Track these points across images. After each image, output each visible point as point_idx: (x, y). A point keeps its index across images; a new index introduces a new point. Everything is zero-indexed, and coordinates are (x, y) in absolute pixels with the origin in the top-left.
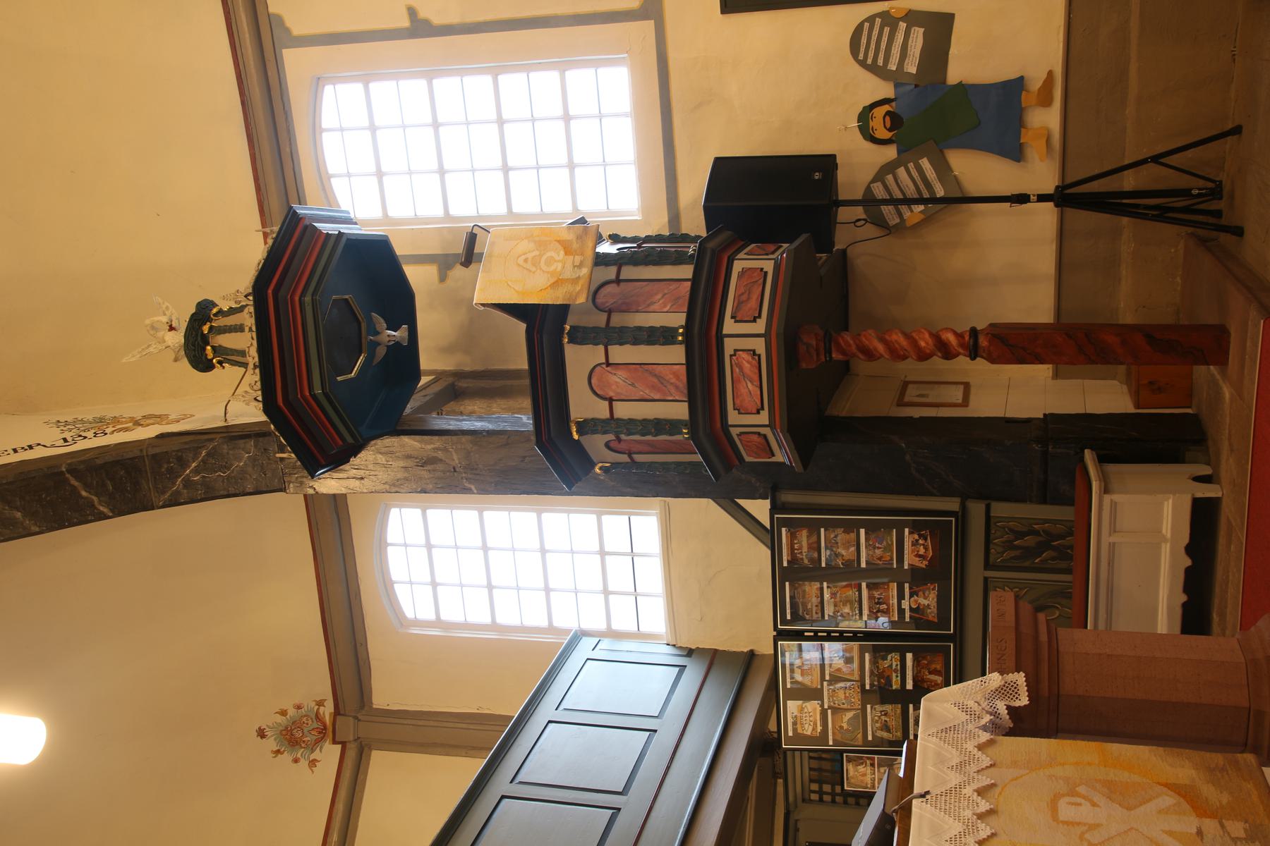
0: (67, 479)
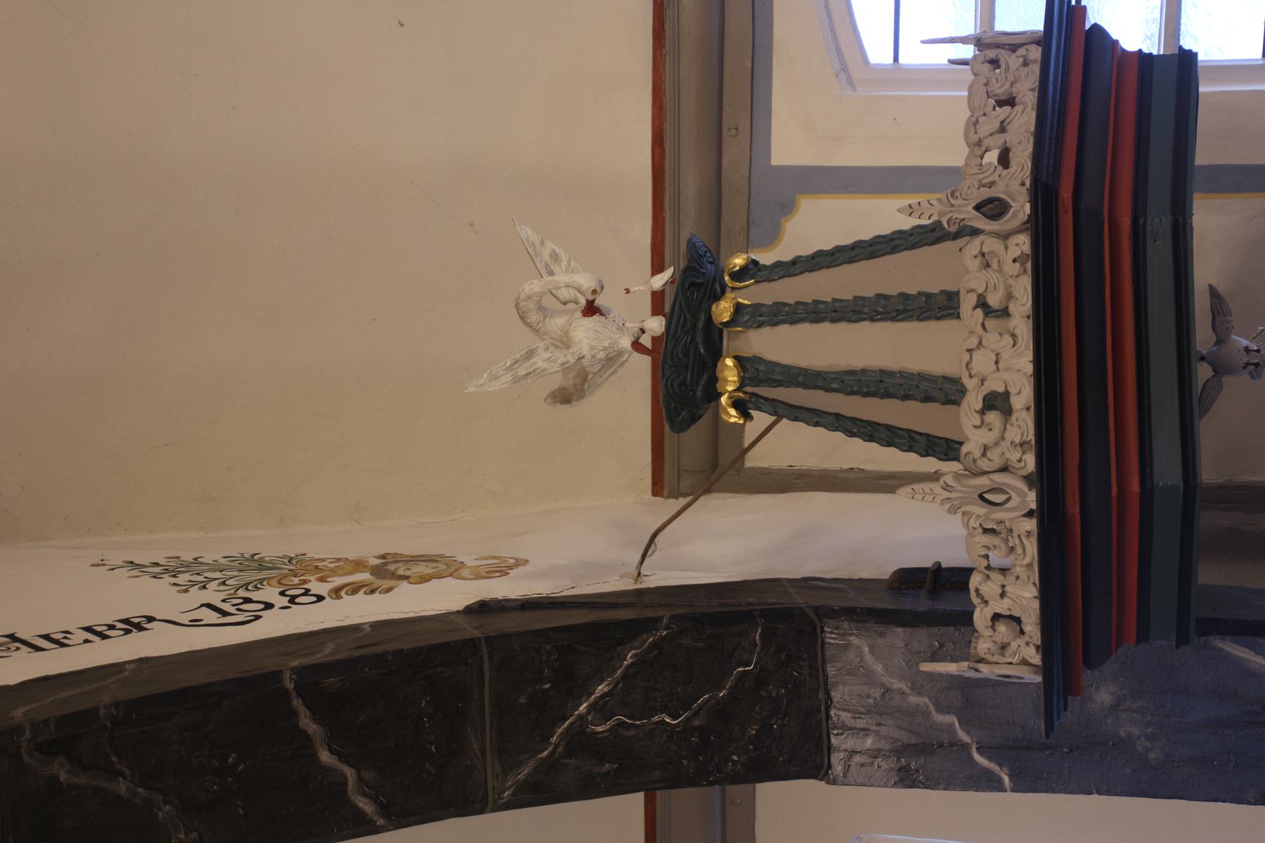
0: (294, 714)
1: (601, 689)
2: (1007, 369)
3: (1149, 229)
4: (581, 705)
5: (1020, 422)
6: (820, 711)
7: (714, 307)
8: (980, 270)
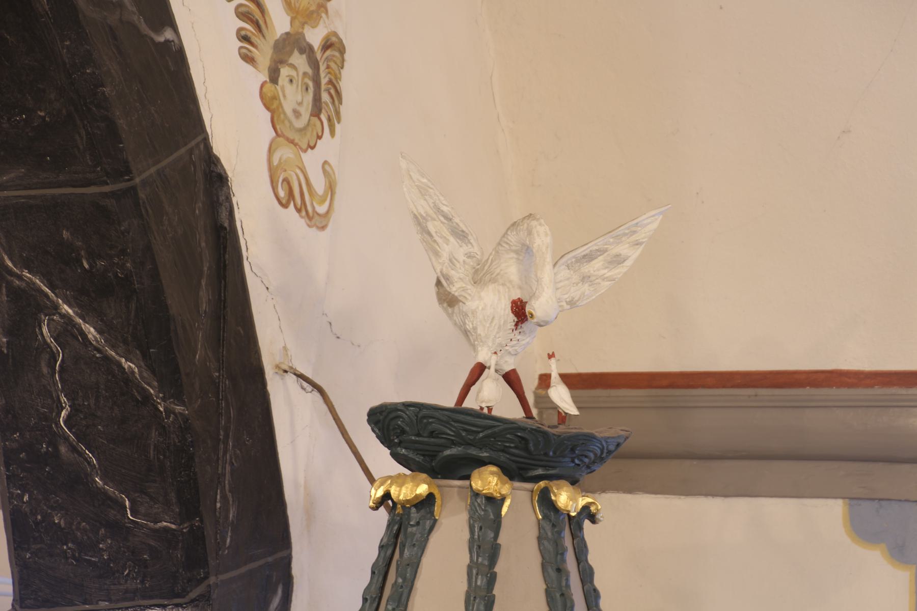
1: (91, 331)
4: (70, 306)
6: (85, 603)
7: (494, 469)
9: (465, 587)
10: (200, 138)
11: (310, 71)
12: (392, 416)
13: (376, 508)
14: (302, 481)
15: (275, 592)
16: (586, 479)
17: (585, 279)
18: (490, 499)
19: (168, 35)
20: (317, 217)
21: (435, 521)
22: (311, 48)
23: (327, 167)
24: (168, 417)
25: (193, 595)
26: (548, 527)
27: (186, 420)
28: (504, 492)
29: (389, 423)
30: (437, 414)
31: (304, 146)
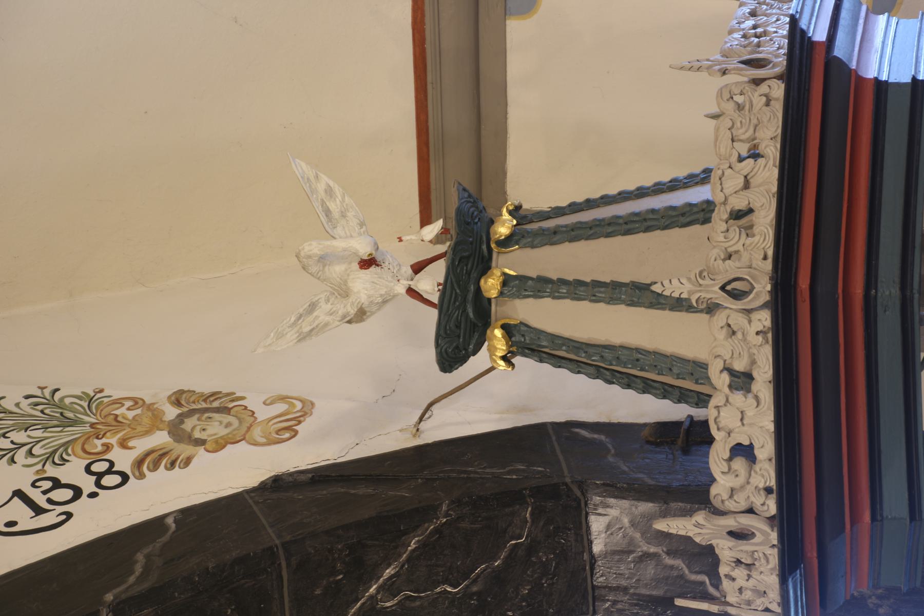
1: (389, 572)
2: (751, 425)
3: (879, 301)
5: (762, 472)
6: (585, 569)
7: (482, 282)
8: (726, 339)
9: (568, 301)
10: (246, 496)
11: (197, 416)
12: (445, 355)
13: (513, 365)
14: (497, 416)
15: (577, 433)
16: (491, 211)
17: (343, 215)
18: (504, 284)
19: (170, 521)
20: (305, 409)
21: (521, 323)
22: (179, 415)
23: (268, 402)
24: (451, 515)
25: (579, 494)
26: (524, 241)
27: (452, 502)
28: (499, 274)
29: (449, 360)
30: (443, 323)
31: (252, 419)
